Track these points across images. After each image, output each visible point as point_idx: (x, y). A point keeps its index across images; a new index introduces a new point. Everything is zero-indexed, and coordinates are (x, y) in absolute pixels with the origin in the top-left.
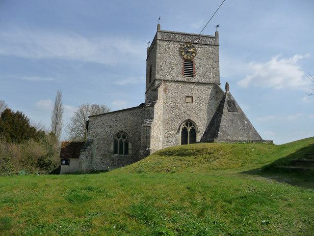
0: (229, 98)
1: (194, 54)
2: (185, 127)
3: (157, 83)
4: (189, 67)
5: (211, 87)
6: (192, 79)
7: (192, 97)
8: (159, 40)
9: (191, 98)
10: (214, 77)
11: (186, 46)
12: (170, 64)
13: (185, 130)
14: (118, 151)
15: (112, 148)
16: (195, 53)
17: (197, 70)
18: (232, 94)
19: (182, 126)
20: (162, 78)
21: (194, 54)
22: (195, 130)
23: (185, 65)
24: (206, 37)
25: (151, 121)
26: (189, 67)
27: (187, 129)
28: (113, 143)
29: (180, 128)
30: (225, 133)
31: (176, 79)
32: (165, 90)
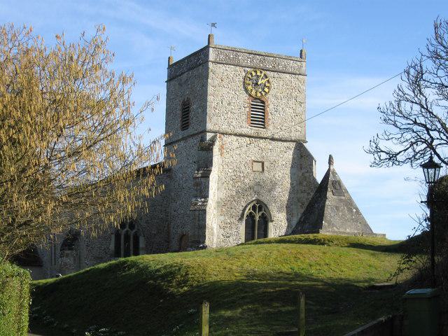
0: (334, 176)
1: (266, 90)
2: (251, 213)
3: (209, 136)
4: (259, 112)
5: (293, 145)
6: (263, 132)
7: (263, 163)
8: (214, 62)
9: (261, 164)
10: (297, 131)
11: (254, 74)
12: (229, 104)
13: (251, 216)
14: (122, 253)
15: (112, 246)
16: (269, 88)
17: (270, 117)
18: (337, 171)
19: (247, 210)
20: (216, 128)
21: (266, 90)
22: (266, 217)
23: (253, 107)
24: (287, 59)
25: (204, 202)
26: (259, 112)
27: (254, 217)
28: (113, 236)
29: (243, 214)
30: (329, 223)
31: (239, 131)
32: (222, 148)
